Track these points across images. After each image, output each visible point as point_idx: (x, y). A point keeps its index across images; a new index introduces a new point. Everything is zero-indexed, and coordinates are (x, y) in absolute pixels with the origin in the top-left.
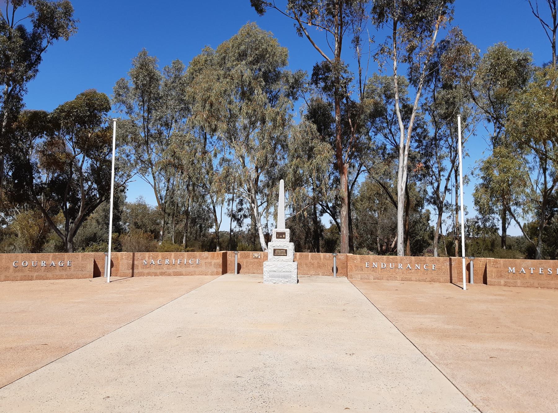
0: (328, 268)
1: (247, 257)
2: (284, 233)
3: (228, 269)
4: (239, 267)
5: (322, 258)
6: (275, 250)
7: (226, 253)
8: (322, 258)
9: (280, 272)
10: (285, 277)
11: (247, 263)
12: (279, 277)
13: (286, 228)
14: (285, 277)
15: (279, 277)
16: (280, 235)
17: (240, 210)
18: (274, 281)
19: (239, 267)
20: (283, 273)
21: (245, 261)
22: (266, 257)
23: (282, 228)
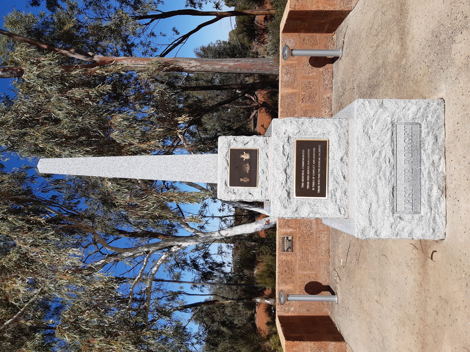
0: (314, 78)
1: (288, 266)
2: (235, 155)
3: (318, 314)
4: (314, 288)
5: (290, 91)
6: (301, 192)
7: (281, 318)
8: (290, 91)
9: (394, 167)
10: (416, 149)
11: (304, 268)
12: (415, 174)
13: (213, 149)
14: (416, 149)
15: (415, 174)
16: (243, 170)
17: (196, 266)
18: (435, 192)
19: (314, 288)
20: (401, 157)
21: (298, 272)
22: (311, 230)
23: (211, 168)
